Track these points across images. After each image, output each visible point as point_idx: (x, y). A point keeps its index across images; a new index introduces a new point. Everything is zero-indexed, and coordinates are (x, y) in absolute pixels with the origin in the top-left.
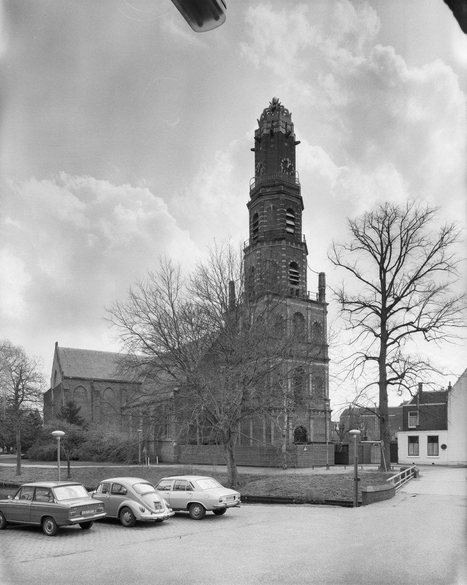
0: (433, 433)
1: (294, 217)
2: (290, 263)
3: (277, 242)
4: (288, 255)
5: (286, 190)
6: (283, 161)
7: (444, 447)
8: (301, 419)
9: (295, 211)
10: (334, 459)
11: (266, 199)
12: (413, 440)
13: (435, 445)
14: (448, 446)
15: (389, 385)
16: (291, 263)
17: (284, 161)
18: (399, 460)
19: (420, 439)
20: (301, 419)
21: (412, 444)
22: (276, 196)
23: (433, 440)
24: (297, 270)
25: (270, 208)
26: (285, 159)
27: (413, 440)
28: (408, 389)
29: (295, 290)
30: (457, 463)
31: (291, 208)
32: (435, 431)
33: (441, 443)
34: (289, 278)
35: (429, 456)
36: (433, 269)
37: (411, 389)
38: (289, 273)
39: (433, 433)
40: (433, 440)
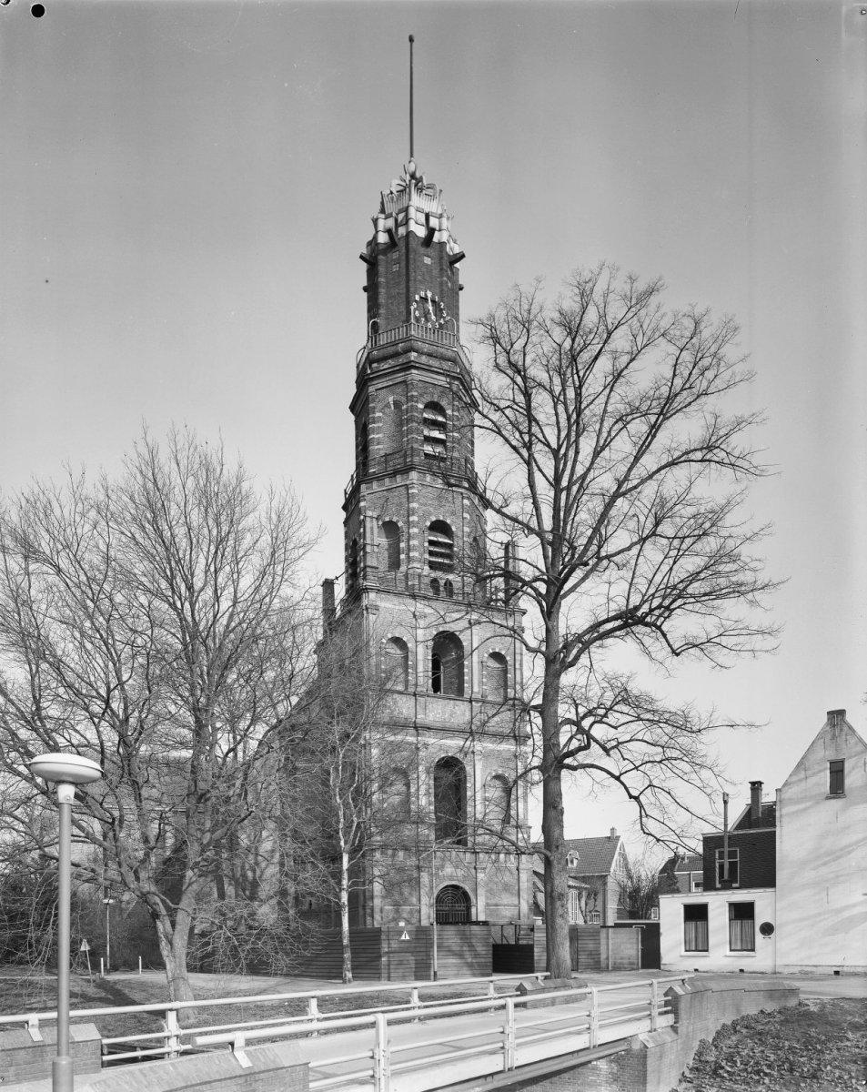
0: (741, 896)
1: (444, 420)
2: (428, 524)
3: (399, 478)
4: (425, 505)
5: (424, 359)
6: (417, 298)
7: (768, 929)
8: (450, 869)
9: (446, 406)
10: (491, 960)
11: (380, 386)
12: (696, 914)
13: (747, 923)
14: (777, 931)
15: (564, 772)
16: (433, 523)
17: (421, 298)
18: (663, 962)
19: (711, 914)
20: (450, 869)
21: (692, 925)
22: (399, 377)
23: (742, 912)
24: (450, 539)
25: (388, 405)
26: (423, 294)
27: (696, 914)
28: (618, 778)
29: (442, 582)
30: (799, 968)
31: (436, 400)
32: (762, 890)
33: (761, 917)
34: (427, 556)
35: (733, 953)
36: (543, 440)
37: (622, 778)
38: (426, 544)
39: (741, 896)
40: (742, 912)
